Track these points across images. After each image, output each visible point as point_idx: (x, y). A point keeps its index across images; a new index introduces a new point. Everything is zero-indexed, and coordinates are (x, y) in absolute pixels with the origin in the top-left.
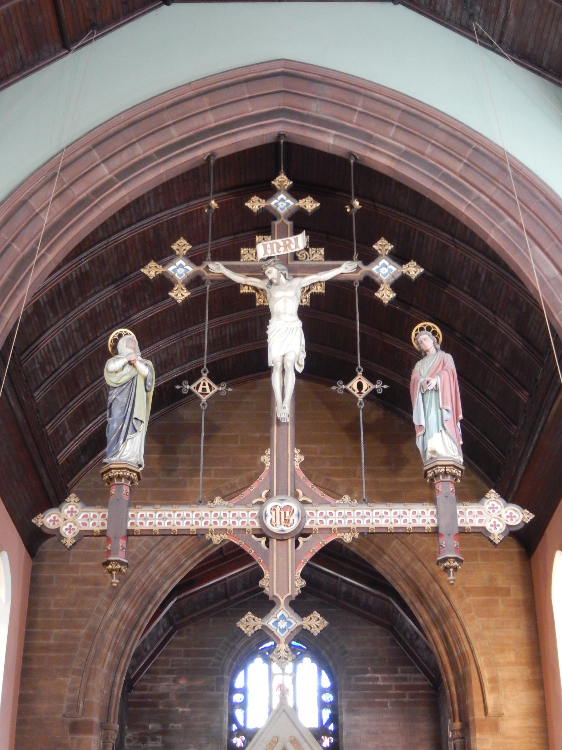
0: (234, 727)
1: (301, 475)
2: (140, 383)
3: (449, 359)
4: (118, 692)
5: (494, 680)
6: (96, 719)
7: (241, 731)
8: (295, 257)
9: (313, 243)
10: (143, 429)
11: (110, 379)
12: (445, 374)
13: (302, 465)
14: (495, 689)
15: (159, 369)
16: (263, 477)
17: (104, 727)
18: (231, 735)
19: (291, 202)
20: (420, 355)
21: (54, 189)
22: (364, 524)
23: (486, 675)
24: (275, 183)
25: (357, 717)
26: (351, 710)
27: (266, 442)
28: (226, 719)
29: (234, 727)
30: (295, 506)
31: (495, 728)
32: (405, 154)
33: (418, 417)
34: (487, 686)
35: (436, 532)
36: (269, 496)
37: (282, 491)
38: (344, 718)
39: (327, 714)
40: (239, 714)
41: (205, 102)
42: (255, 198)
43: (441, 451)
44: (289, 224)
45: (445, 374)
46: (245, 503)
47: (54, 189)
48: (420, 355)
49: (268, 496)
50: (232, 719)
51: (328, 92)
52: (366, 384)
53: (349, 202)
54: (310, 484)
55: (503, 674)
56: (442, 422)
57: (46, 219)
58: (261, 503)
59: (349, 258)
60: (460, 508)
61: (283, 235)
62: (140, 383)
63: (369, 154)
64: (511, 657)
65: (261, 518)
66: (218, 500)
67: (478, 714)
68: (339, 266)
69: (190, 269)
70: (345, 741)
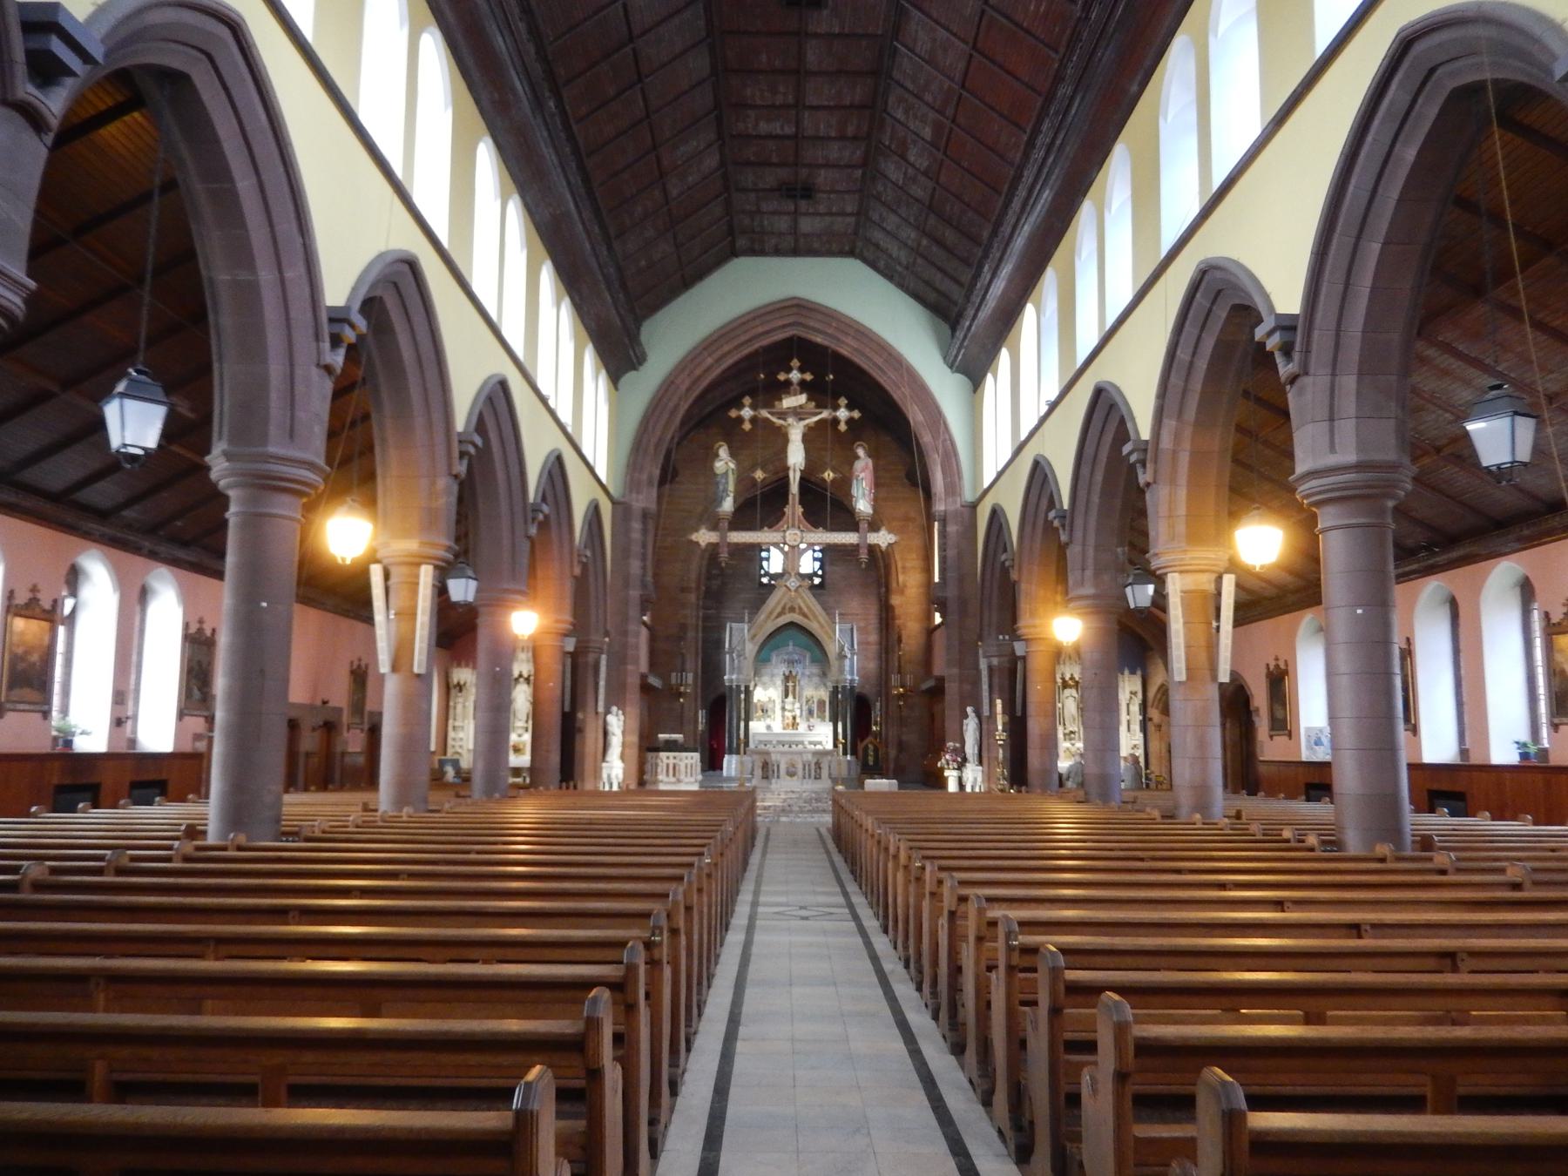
0: (762, 572)
1: (802, 518)
2: (730, 473)
3: (870, 462)
4: (704, 570)
5: (904, 568)
6: (693, 585)
7: (767, 574)
8: (801, 407)
9: (809, 399)
10: (732, 495)
11: (718, 472)
12: (867, 471)
13: (803, 514)
14: (903, 573)
15: (738, 464)
16: (785, 518)
17: (698, 588)
18: (761, 576)
19: (799, 375)
20: (857, 458)
21: (686, 373)
22: (828, 541)
23: (900, 565)
24: (792, 364)
25: (836, 568)
26: (832, 564)
27: (786, 502)
28: (758, 568)
29: (762, 572)
30: (798, 532)
31: (902, 592)
32: (856, 350)
33: (854, 492)
34: (900, 570)
35: (858, 545)
36: (788, 528)
37: (793, 526)
38: (827, 568)
39: (817, 564)
40: (765, 564)
41: (758, 322)
42: (782, 373)
43: (862, 508)
44: (798, 388)
45: (867, 471)
46: (775, 531)
47: (686, 373)
48: (857, 458)
49: (788, 528)
50: (762, 568)
51: (819, 317)
52: (831, 474)
53: (828, 375)
54: (806, 523)
55: (908, 565)
56: (864, 495)
57: (683, 388)
58: (784, 531)
59: (825, 407)
60: (869, 535)
61: (795, 395)
62: (730, 473)
63: (838, 348)
64: (914, 556)
65: (784, 537)
66: (766, 528)
67: (894, 585)
68: (820, 413)
69: (752, 413)
70: (828, 581)
